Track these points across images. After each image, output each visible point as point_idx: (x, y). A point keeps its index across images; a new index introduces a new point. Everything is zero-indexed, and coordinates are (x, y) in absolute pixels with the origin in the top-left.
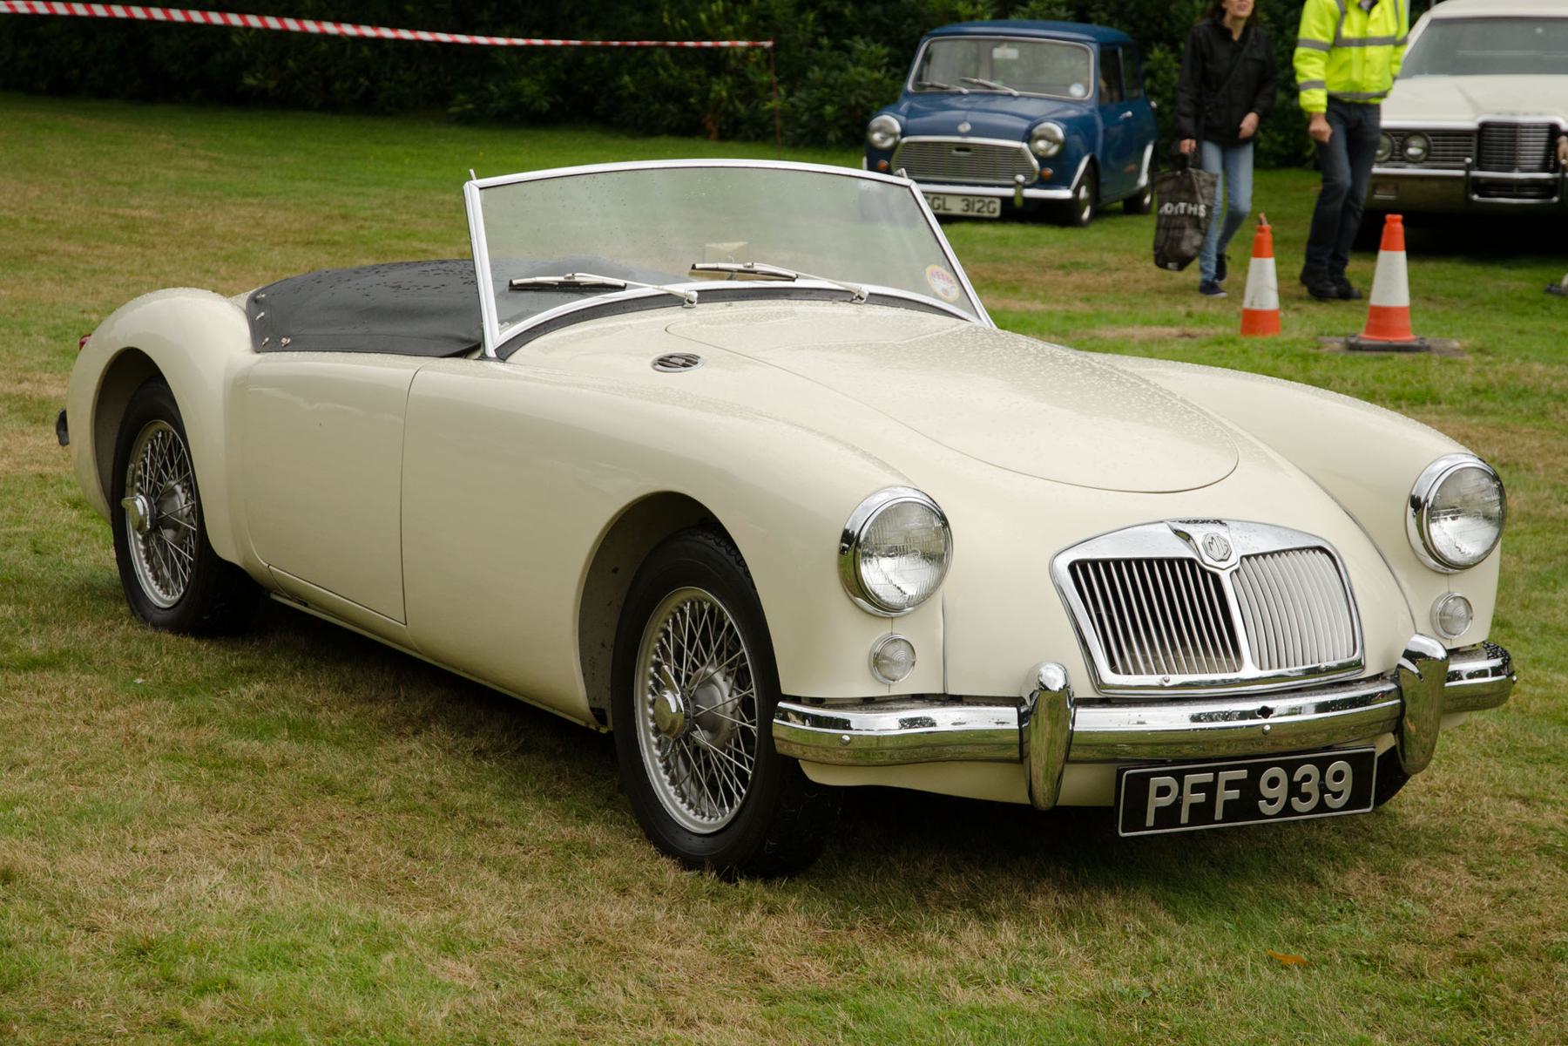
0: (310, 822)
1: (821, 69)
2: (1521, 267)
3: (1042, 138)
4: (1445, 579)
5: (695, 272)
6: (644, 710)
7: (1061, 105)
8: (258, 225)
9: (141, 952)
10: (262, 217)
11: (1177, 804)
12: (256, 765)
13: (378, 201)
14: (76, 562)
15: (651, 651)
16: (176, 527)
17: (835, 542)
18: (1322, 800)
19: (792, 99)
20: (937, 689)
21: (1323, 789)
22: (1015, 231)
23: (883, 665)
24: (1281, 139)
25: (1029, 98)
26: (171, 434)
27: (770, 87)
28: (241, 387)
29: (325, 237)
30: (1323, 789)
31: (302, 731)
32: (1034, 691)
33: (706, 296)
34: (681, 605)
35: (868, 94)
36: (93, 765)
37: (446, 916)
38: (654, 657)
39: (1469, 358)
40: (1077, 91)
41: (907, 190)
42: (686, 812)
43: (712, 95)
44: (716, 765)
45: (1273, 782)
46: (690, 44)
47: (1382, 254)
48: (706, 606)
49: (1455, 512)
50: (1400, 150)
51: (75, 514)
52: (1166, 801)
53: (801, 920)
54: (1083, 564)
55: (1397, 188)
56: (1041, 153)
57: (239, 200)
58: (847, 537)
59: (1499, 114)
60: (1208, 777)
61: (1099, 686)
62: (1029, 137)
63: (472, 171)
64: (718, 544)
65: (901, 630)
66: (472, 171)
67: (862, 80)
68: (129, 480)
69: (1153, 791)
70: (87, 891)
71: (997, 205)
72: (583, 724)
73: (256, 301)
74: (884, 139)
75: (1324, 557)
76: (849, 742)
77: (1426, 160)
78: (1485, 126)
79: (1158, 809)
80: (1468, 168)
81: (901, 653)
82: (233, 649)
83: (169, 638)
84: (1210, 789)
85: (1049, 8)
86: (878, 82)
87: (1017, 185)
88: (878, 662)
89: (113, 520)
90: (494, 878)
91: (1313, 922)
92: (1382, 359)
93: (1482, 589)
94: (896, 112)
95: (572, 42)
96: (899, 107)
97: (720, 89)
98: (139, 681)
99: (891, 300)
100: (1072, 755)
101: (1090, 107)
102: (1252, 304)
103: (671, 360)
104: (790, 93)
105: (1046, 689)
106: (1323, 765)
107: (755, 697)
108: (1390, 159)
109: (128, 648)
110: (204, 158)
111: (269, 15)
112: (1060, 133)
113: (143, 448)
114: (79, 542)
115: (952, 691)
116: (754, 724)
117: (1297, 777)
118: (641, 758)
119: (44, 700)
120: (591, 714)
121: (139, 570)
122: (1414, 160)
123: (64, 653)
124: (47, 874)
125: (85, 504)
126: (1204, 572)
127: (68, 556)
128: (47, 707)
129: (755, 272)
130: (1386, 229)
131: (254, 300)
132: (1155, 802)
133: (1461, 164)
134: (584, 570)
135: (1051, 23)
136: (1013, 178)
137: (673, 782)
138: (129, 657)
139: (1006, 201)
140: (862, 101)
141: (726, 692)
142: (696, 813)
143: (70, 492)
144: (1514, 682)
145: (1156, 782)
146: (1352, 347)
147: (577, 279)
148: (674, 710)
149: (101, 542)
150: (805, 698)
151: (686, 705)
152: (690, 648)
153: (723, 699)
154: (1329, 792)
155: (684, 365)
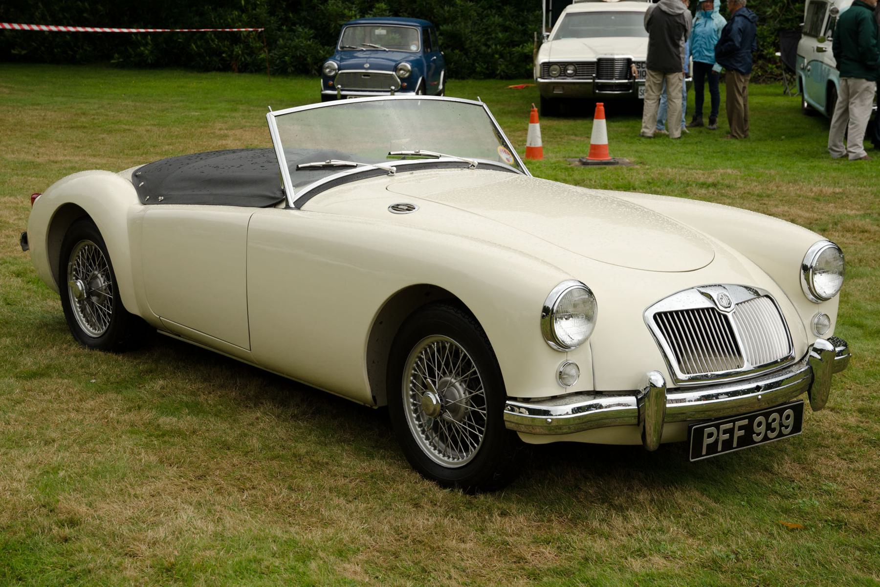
0: (225, 469)
1: (283, 40)
2: (617, 121)
3: (401, 69)
4: (817, 305)
5: (391, 156)
6: (408, 400)
7: (408, 55)
8: (44, 119)
9: (168, 570)
10: (45, 115)
11: (716, 441)
12: (179, 433)
13: (96, 106)
14: (31, 309)
15: (411, 368)
16: (98, 295)
17: (539, 312)
18: (780, 430)
19: (271, 54)
23: (564, 378)
24: (485, 66)
25: (393, 51)
26: (93, 248)
27: (261, 49)
28: (137, 224)
29: (79, 124)
30: (781, 425)
31: (196, 409)
32: (647, 387)
33: (401, 169)
34: (430, 344)
35: (305, 51)
36: (91, 439)
37: (330, 531)
38: (413, 371)
39: (638, 167)
40: (414, 48)
41: (482, 108)
42: (438, 455)
43: (235, 53)
44: (462, 431)
45: (760, 424)
46: (228, 30)
47: (596, 121)
48: (448, 346)
49: (823, 271)
50: (564, 71)
51: (19, 280)
52: (711, 440)
53: (521, 519)
54: (659, 314)
55: (563, 88)
56: (401, 76)
57: (31, 107)
58: (546, 310)
59: (606, 54)
60: (730, 425)
61: (675, 380)
62: (396, 69)
63: (269, 107)
64: (464, 317)
65: (571, 358)
66: (269, 107)
67: (302, 45)
68: (69, 271)
69: (705, 435)
72: (362, 404)
73: (136, 176)
74: (330, 72)
75: (768, 300)
76: (551, 422)
77: (575, 75)
78: (600, 60)
80: (594, 78)
81: (572, 371)
82: (135, 358)
83: (98, 353)
84: (731, 431)
85: (381, 11)
86: (310, 46)
88: (561, 375)
89: (60, 292)
90: (342, 501)
91: (788, 498)
92: (601, 169)
93: (832, 309)
94: (335, 60)
95: (166, 30)
96: (335, 57)
97: (238, 50)
98: (94, 381)
99: (485, 166)
100: (665, 420)
101: (420, 55)
102: (530, 144)
103: (399, 207)
104: (270, 51)
105: (655, 386)
106: (781, 412)
107: (484, 396)
108: (560, 76)
110: (6, 87)
111: (14, 23)
112: (409, 66)
113: (76, 254)
114: (29, 297)
115: (598, 389)
116: (484, 409)
117: (770, 421)
118: (408, 426)
119: (47, 397)
120: (372, 399)
121: (77, 318)
122: (570, 76)
123: (48, 367)
124: (93, 517)
125: (22, 274)
126: (719, 314)
127: (25, 305)
128: (50, 401)
129: (420, 155)
130: (596, 109)
131: (135, 175)
132: (707, 441)
133: (591, 77)
134: (371, 323)
135: (383, 18)
136: (390, 88)
137: (427, 438)
138: (82, 367)
140: (303, 54)
141: (462, 392)
142: (444, 456)
143: (13, 268)
144: (851, 356)
145: (707, 431)
146: (585, 164)
147: (332, 163)
148: (435, 402)
149: (40, 296)
150: (519, 398)
151: (441, 400)
152: (439, 369)
153: (460, 396)
154: (784, 426)
155: (407, 210)
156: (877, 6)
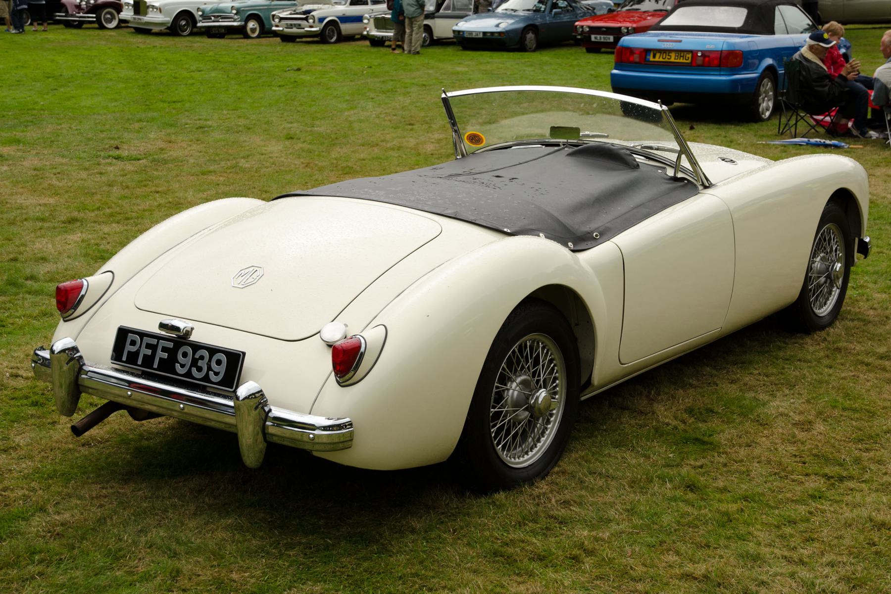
20: (454, 216)
21: (210, 368)
52: (133, 349)
70: (68, 519)
79: (129, 352)
117: (197, 356)
137: (539, 441)
154: (212, 370)
156: (873, 100)
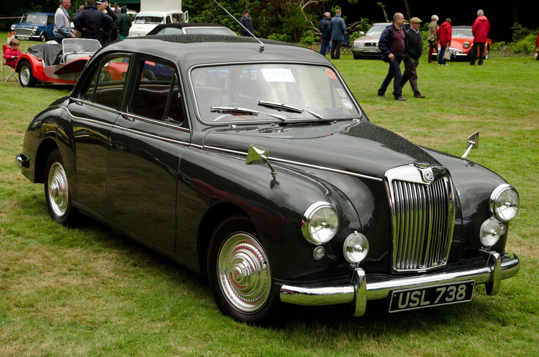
22: (456, 64)
63: (511, 28)
66: (511, 28)
71: (28, 38)
87: (31, 35)
109: (56, 285)
117: (448, 290)
139: (30, 37)
